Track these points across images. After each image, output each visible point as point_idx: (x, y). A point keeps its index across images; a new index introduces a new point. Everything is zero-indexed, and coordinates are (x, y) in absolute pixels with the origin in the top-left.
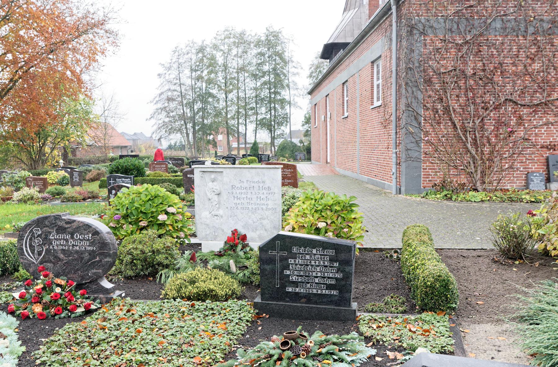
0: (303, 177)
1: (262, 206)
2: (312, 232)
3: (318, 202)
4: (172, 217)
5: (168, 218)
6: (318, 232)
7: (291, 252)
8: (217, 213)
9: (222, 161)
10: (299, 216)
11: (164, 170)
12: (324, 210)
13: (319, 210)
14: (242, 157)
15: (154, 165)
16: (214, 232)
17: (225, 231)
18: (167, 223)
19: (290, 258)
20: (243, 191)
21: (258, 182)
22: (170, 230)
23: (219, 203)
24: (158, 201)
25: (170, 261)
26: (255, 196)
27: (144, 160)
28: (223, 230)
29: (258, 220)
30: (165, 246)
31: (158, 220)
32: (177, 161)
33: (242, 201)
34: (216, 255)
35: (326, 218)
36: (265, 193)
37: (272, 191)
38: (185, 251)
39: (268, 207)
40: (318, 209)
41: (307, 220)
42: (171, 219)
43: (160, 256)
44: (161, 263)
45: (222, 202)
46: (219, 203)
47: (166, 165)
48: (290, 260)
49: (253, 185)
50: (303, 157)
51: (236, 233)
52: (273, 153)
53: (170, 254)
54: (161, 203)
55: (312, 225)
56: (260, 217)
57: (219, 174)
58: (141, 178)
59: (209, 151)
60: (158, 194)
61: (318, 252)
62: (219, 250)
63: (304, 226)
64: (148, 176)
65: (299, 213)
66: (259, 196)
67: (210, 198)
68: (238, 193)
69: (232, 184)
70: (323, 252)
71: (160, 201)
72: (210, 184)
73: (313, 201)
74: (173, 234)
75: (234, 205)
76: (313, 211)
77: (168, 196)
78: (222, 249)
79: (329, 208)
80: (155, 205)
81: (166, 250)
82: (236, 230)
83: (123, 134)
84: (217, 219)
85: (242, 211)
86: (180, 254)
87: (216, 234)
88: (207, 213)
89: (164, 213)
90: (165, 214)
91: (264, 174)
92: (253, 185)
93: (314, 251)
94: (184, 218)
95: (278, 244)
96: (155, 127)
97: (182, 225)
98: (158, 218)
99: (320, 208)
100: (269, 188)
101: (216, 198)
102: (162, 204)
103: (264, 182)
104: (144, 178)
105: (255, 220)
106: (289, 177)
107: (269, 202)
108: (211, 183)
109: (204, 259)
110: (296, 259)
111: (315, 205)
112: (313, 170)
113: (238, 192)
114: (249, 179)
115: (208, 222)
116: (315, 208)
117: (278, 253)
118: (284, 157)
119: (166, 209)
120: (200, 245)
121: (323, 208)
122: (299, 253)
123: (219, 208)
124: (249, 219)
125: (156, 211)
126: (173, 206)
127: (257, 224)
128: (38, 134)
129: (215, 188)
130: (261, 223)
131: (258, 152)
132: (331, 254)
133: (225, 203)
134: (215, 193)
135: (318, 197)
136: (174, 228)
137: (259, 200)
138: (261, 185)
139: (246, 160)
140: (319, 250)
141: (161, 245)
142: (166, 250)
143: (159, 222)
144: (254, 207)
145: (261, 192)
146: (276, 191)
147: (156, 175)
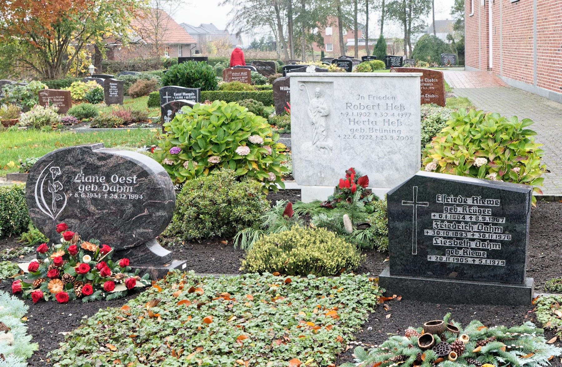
0: (453, 90)
2: (466, 172)
3: (476, 127)
4: (256, 150)
5: (251, 152)
6: (474, 173)
7: (435, 202)
8: (324, 144)
10: (447, 149)
11: (246, 79)
13: (477, 139)
14: (361, 60)
15: (231, 72)
16: (320, 172)
17: (336, 170)
18: (249, 159)
19: (434, 212)
20: (363, 111)
21: (386, 98)
22: (254, 169)
24: (236, 126)
26: (381, 119)
27: (215, 65)
28: (333, 170)
29: (385, 155)
31: (236, 154)
33: (362, 126)
35: (487, 152)
36: (396, 114)
37: (406, 111)
38: (277, 201)
39: (401, 135)
40: (475, 138)
41: (459, 154)
43: (239, 208)
44: (240, 219)
48: (433, 214)
49: (378, 101)
51: (352, 175)
52: (408, 54)
53: (253, 206)
54: (241, 130)
55: (466, 161)
56: (388, 150)
57: (327, 86)
58: (210, 91)
60: (236, 116)
61: (475, 202)
62: (327, 200)
63: (454, 164)
65: (447, 145)
67: (314, 121)
68: (355, 114)
69: (346, 101)
70: (483, 203)
71: (240, 126)
72: (314, 101)
73: (468, 127)
74: (258, 175)
75: (349, 133)
76: (468, 141)
78: (331, 197)
79: (491, 136)
80: (232, 132)
82: (352, 170)
83: (184, 26)
84: (324, 153)
87: (323, 176)
88: (310, 143)
89: (245, 143)
90: (247, 145)
91: (394, 86)
92: (378, 101)
93: (470, 201)
94: (275, 151)
95: (415, 190)
96: (232, 16)
97: (271, 162)
98: (237, 151)
99: (478, 136)
100: (402, 107)
101: (322, 121)
102: (243, 130)
104: (215, 91)
107: (402, 128)
108: (315, 100)
109: (305, 212)
110: (443, 212)
111: (470, 132)
113: (355, 112)
114: (371, 93)
115: (311, 157)
117: (415, 203)
118: (424, 60)
119: (247, 138)
120: (299, 191)
121: (482, 137)
122: (446, 204)
123: (327, 136)
124: (372, 152)
125: (233, 141)
126: (258, 134)
127: (384, 160)
128: (56, 25)
129: (321, 106)
130: (390, 159)
131: (385, 53)
132: (494, 205)
133: (336, 130)
134: (321, 114)
135: (475, 120)
136: (259, 166)
137: (386, 124)
138: (390, 102)
139: (368, 65)
140: (477, 200)
141: (241, 192)
143: (237, 158)
144: (379, 135)
145: (390, 112)
147: (233, 87)
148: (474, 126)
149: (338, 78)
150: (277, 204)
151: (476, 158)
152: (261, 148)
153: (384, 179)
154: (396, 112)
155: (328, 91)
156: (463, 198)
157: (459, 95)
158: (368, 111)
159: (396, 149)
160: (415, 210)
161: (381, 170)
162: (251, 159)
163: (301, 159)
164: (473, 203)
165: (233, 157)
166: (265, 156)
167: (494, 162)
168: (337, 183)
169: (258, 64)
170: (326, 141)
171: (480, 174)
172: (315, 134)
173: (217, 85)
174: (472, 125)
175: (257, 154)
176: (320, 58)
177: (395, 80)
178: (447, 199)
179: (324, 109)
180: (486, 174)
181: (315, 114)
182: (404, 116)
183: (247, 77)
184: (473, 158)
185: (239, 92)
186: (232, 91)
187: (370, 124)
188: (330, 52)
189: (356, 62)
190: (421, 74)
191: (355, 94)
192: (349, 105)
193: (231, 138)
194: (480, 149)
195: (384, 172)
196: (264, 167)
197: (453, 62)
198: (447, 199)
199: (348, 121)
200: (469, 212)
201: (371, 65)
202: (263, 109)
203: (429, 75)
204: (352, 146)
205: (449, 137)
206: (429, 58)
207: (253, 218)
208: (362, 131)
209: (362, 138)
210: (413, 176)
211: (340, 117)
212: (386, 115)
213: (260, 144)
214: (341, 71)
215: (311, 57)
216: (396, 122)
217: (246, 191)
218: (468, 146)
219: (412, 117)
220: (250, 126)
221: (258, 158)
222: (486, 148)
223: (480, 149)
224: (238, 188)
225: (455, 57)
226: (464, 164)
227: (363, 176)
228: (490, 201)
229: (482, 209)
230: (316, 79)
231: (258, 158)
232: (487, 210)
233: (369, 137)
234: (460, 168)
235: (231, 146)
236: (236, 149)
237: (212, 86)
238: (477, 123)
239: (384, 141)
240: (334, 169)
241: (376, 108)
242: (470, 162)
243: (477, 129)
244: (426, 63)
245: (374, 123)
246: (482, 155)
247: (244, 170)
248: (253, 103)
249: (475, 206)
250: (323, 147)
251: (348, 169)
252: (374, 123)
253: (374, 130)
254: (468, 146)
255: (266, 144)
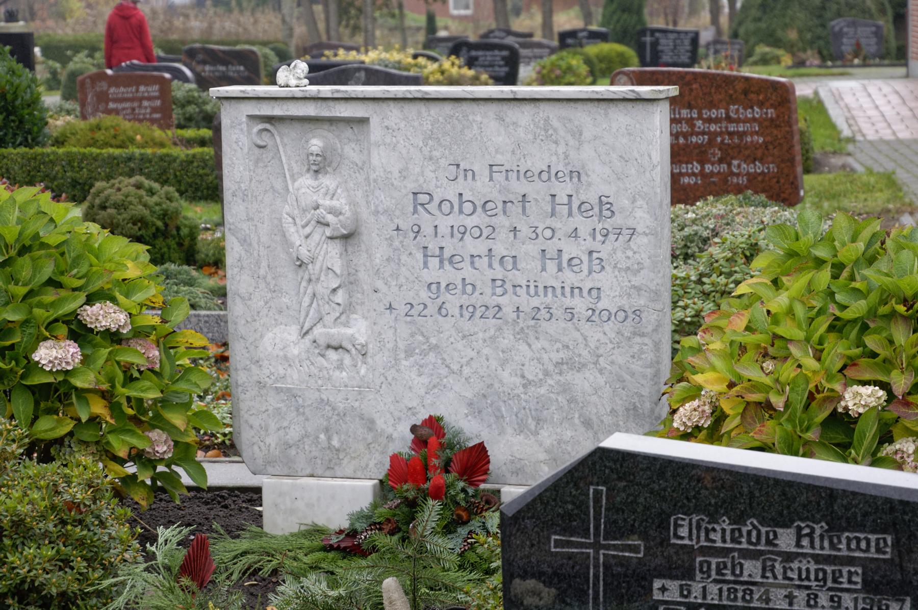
0: (850, 147)
1: (568, 302)
2: (810, 435)
3: (852, 278)
4: (104, 352)
5: (86, 360)
6: (841, 438)
7: (664, 542)
8: (339, 332)
9: (447, 65)
10: (751, 354)
11: (154, 110)
12: (880, 323)
13: (855, 321)
14: (555, 43)
15: (104, 85)
16: (327, 430)
17: (380, 424)
18: (79, 383)
19: (661, 576)
20: (470, 222)
21: (547, 174)
22: (94, 420)
23: (350, 282)
24: (36, 269)
25: (83, 578)
26: (533, 249)
27: (70, 59)
28: (370, 424)
29: (547, 373)
30: (56, 500)
31: (33, 367)
32: (225, 63)
33: (467, 271)
34: (328, 548)
35: (888, 364)
36: (584, 231)
37: (618, 220)
38: (160, 530)
39: (601, 305)
40: (847, 315)
41: (788, 372)
42: (101, 362)
43: (30, 551)
44: (34, 589)
45: (362, 275)
46: (350, 282)
47: (165, 86)
48: (657, 584)
49: (519, 187)
50: (870, 45)
51: (433, 440)
52: (724, 20)
53: (81, 543)
54: (53, 283)
55: (811, 397)
56: (556, 357)
57: (348, 132)
58: (23, 150)
59: (402, 15)
60: (36, 236)
61: (805, 542)
62: (346, 525)
63: (768, 406)
64: (59, 142)
65: (750, 339)
66: (552, 247)
67: (304, 253)
68: (444, 229)
69: (412, 186)
70: (833, 546)
71: (48, 271)
73: (824, 276)
74: (111, 438)
75: (424, 295)
76: (822, 325)
77: (87, 244)
78: (360, 516)
79: (901, 309)
80: (22, 291)
81: (63, 522)
82: (434, 423)
84: (340, 367)
85: (467, 326)
86: (136, 544)
87: (335, 443)
88: (291, 333)
89: (63, 330)
90: (74, 336)
91: (577, 134)
92: (519, 187)
93: (786, 540)
94: (171, 359)
95: (597, 500)
97: (158, 395)
98: (36, 357)
99: (857, 308)
100: (605, 206)
101: (332, 254)
102: (59, 285)
103: (576, 174)
104: (38, 150)
105: (532, 371)
106: (756, 146)
107: (605, 280)
108: (306, 181)
109: (268, 568)
110: (692, 578)
111: (832, 294)
112: (906, 112)
113: (444, 224)
114: (499, 159)
115: (294, 378)
116: (833, 309)
117: (597, 546)
118: (776, 43)
119: (74, 314)
120: (254, 494)
121: (872, 313)
122: (704, 551)
123: (349, 308)
124: (503, 363)
125: (25, 323)
126: (113, 300)
127: (543, 391)
129: (327, 202)
130: (565, 388)
131: (641, 21)
132: (873, 554)
133: (379, 284)
134: (328, 232)
135: (851, 251)
136: (114, 408)
137: (551, 266)
138: (563, 190)
139: (576, 62)
140: (810, 535)
141: (36, 495)
142: (63, 522)
143: (37, 380)
144: (527, 302)
145: (563, 225)
146: (642, 218)
147: (100, 136)
148: (845, 274)
149: (384, 106)
150: (161, 540)
151: (846, 386)
152: (124, 346)
153: (542, 456)
154: (584, 225)
155: (351, 151)
156: (763, 530)
157: (869, 163)
158: (487, 219)
159: (585, 353)
160: (596, 566)
161: (532, 424)
162: (86, 386)
163: (260, 384)
164: (798, 545)
165: (23, 377)
166: (136, 374)
167: (911, 399)
168: (379, 466)
169: (200, 57)
170: (346, 325)
171: (861, 443)
172: (306, 300)
173: (46, 130)
174: (838, 268)
175: (108, 368)
176: (421, 37)
177: (582, 116)
178: (707, 531)
179: (333, 211)
180: (881, 443)
181: (308, 230)
182: (612, 237)
183: (158, 103)
184: (838, 387)
185: (117, 152)
186: (95, 150)
187: (496, 265)
188: (461, 18)
189: (537, 51)
190: (673, 90)
191: (443, 162)
192: (423, 198)
193: (14, 311)
194: (863, 355)
195: (544, 433)
196: (131, 412)
197: (873, 49)
198: (707, 531)
199: (419, 256)
200: (786, 578)
201: (588, 61)
202: (177, 213)
203: (745, 93)
204: (433, 341)
205: (759, 311)
206: (793, 35)
207: (75, 587)
208: (469, 289)
209: (467, 315)
210: (388, 459)
211: (391, 239)
212: (548, 233)
213: (117, 333)
214: (475, 81)
215: (398, 34)
216: (585, 258)
217: (57, 493)
218: (821, 343)
219: (641, 241)
220: (84, 269)
221: (111, 381)
222: (883, 353)
223: (863, 355)
224: (26, 482)
225: (878, 33)
226: (807, 407)
227: (471, 444)
228: (858, 540)
229: (829, 569)
230: (310, 110)
231: (111, 381)
232: (845, 570)
233: (492, 312)
234: (790, 420)
235: (16, 340)
236: (34, 349)
237: (29, 132)
238: (856, 262)
239: (544, 324)
240: (372, 422)
241: (512, 209)
242: (827, 399)
243: (857, 285)
244: (780, 52)
245: (509, 261)
246: (867, 377)
247: (59, 421)
248: (142, 192)
249: (804, 555)
250: (334, 343)
251: (419, 420)
252: (509, 261)
253: (508, 286)
254: (821, 343)
255: (140, 333)
